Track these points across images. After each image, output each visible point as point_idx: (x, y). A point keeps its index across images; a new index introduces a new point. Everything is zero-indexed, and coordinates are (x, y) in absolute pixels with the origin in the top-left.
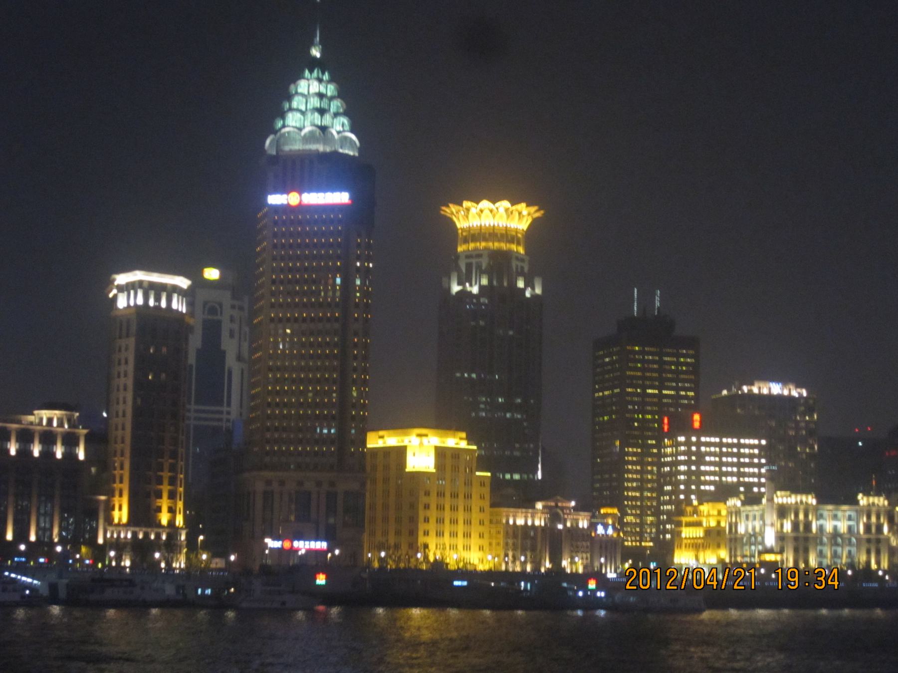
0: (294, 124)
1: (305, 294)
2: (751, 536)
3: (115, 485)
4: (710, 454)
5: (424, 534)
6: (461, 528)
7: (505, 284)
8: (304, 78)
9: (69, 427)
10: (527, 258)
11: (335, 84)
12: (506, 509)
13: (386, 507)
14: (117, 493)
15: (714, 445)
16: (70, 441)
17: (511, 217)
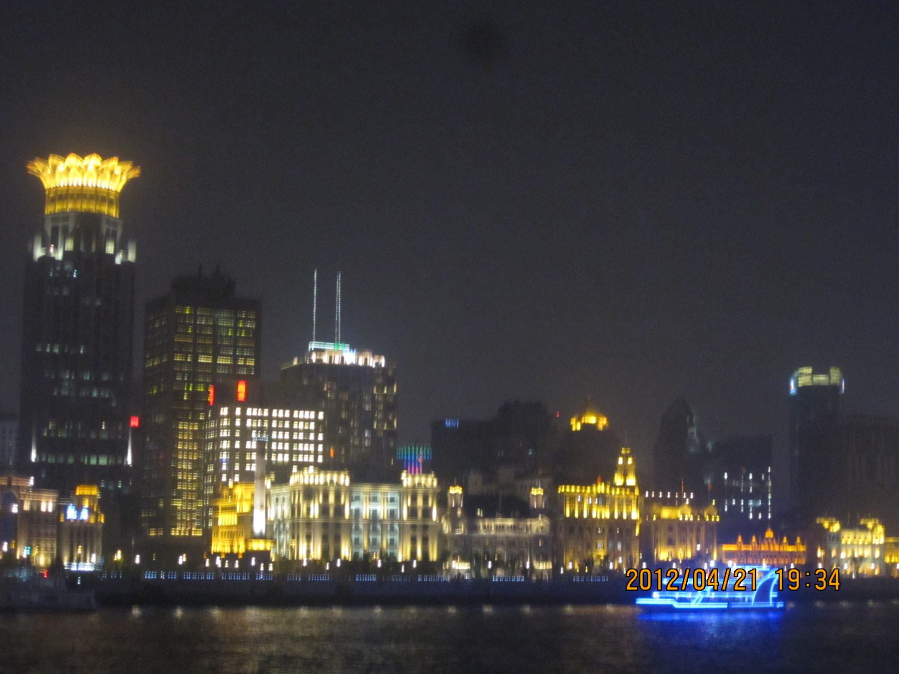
2: (279, 522)
10: (121, 223)
17: (101, 176)
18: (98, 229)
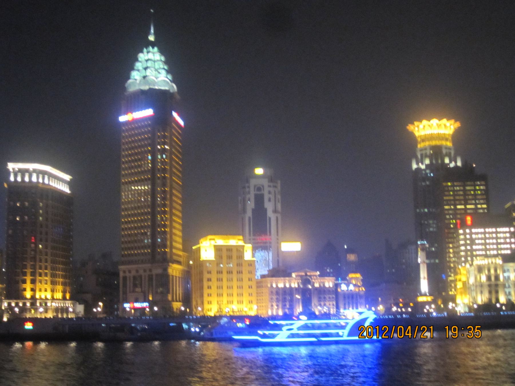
4: (479, 239)
6: (235, 291)
15: (481, 233)
18: (441, 152)
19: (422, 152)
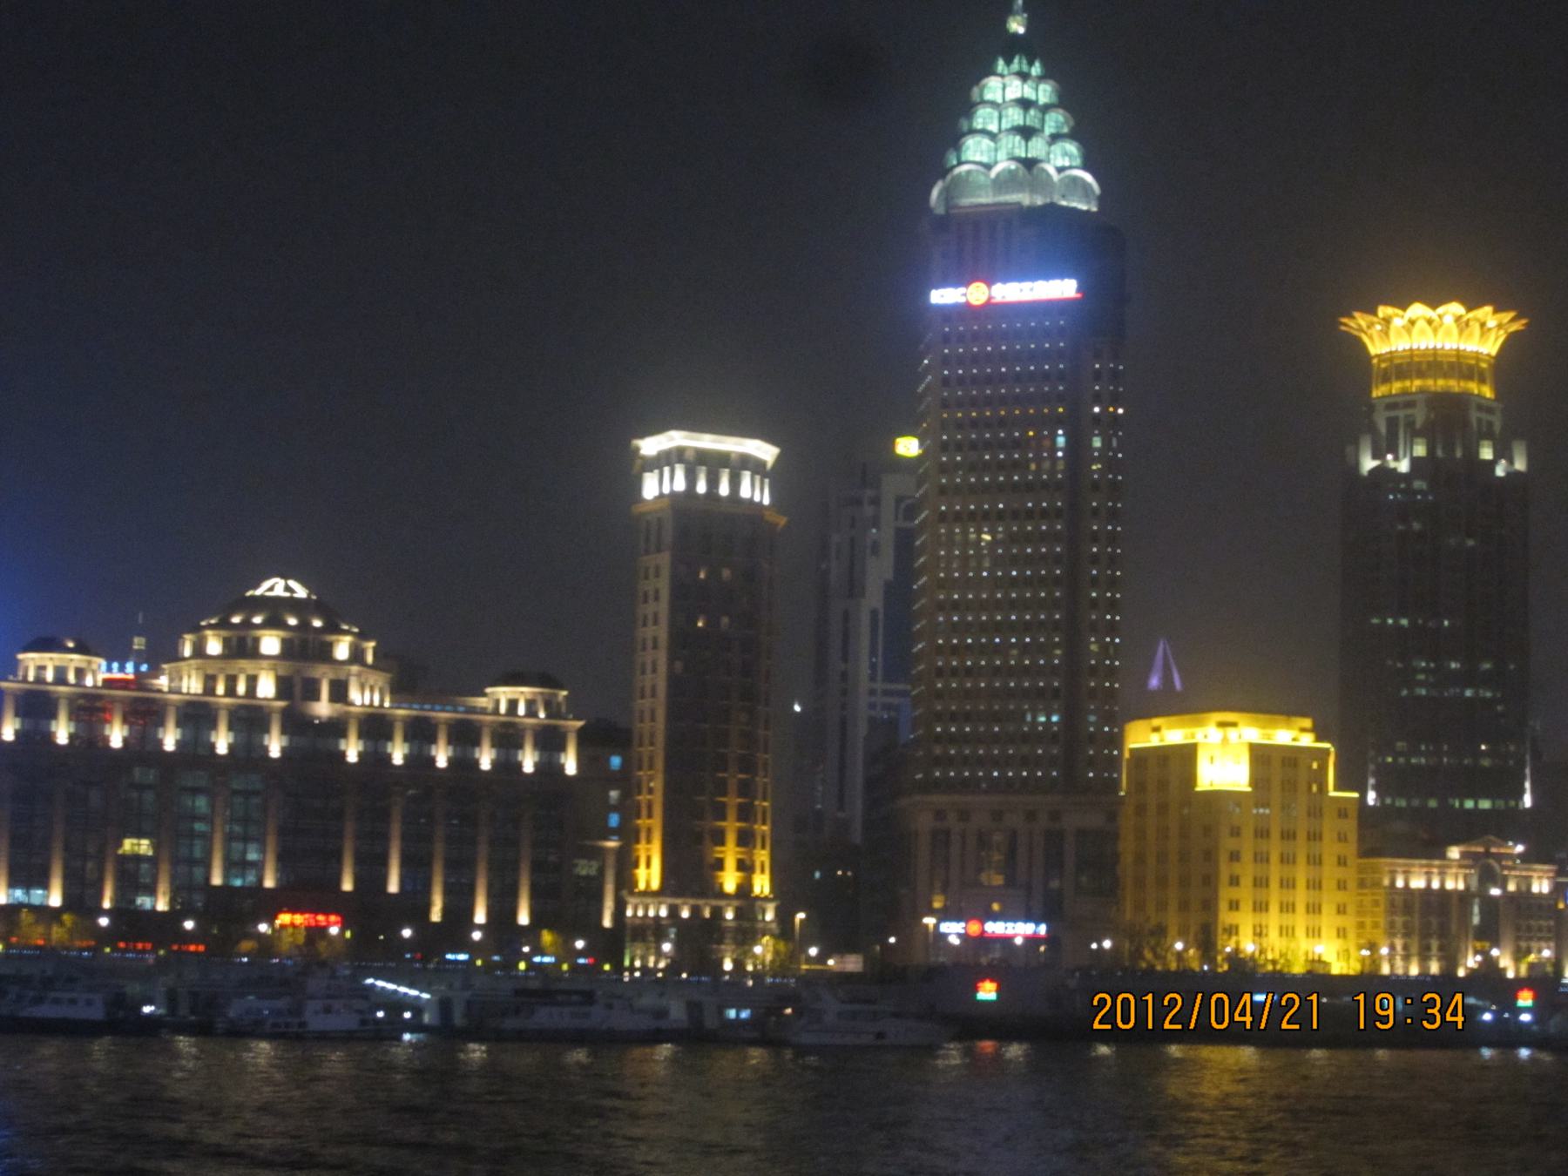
0: (978, 158)
1: (1001, 466)
3: (639, 822)
5: (1231, 908)
6: (1301, 896)
7: (1459, 454)
8: (995, 74)
9: (548, 716)
11: (1052, 82)
12: (1389, 860)
13: (1162, 857)
14: (643, 835)
16: (550, 742)
17: (1466, 332)
18: (1466, 423)
19: (1393, 414)
